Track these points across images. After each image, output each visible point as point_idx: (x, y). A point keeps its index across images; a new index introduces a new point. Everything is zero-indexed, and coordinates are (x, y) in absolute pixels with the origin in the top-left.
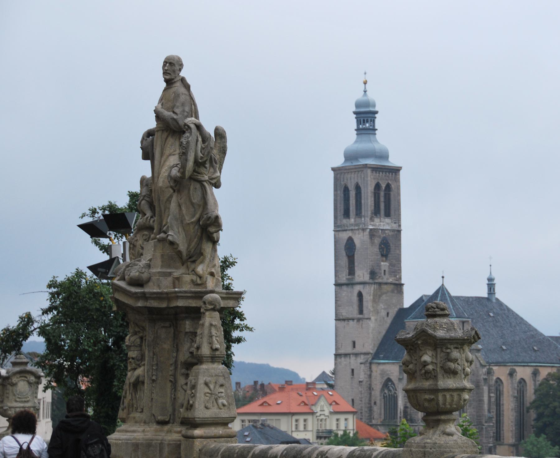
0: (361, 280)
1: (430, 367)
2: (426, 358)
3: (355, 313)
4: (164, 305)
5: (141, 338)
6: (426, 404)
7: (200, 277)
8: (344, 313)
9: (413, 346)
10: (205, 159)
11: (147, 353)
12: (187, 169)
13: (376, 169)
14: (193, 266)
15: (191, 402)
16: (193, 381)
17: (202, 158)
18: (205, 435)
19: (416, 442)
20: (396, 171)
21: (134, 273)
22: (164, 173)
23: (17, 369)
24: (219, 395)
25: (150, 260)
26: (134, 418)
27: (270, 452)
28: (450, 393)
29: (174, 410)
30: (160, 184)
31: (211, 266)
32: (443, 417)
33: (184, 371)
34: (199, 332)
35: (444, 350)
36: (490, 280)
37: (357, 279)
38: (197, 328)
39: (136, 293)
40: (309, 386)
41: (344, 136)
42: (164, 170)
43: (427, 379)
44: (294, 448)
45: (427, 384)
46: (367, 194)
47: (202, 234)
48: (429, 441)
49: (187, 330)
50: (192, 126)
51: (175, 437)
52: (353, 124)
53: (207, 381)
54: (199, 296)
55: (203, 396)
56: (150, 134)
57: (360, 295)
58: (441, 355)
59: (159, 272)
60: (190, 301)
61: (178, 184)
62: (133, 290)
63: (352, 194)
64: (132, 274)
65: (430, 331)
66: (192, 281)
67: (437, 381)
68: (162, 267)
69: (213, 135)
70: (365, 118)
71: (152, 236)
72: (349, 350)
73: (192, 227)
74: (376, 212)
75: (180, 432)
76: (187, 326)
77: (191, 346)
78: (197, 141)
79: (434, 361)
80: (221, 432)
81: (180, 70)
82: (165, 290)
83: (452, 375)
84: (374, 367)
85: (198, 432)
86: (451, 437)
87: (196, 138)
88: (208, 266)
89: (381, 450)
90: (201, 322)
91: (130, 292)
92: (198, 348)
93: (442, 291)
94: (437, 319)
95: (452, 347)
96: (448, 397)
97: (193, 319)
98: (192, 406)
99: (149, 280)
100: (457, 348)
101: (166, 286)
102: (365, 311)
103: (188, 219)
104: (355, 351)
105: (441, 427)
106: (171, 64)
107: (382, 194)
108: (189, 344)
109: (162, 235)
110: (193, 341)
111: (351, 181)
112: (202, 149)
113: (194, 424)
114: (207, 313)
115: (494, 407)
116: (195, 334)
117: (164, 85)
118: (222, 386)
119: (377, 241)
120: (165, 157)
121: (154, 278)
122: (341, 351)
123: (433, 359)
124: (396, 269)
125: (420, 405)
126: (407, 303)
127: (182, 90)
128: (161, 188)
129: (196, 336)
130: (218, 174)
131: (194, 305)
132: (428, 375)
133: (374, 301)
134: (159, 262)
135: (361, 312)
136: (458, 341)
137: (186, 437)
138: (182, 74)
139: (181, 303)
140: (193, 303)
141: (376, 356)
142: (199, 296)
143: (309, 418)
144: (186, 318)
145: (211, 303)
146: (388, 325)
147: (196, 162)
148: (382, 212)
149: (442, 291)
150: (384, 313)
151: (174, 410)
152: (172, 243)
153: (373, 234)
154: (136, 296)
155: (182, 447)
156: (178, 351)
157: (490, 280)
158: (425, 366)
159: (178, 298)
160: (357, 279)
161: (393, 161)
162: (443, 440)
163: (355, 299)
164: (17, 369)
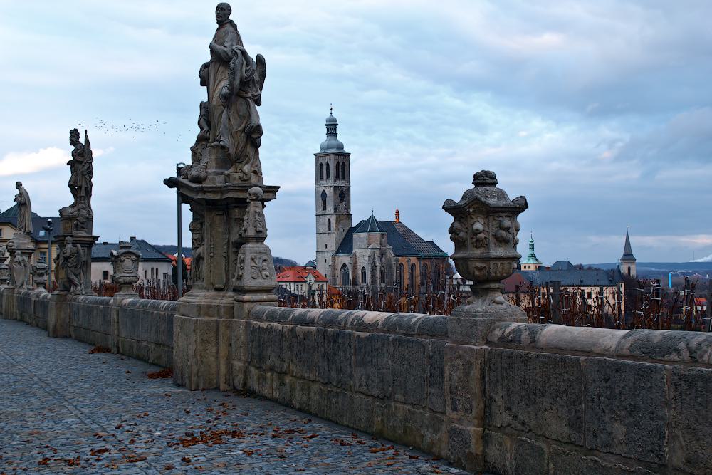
0: (330, 212)
1: (482, 235)
2: (478, 226)
3: (327, 230)
4: (218, 197)
5: (201, 224)
6: (477, 273)
7: (246, 175)
8: (322, 231)
9: (464, 214)
10: (249, 79)
11: (205, 235)
12: (235, 86)
13: (336, 154)
14: (240, 166)
15: (240, 273)
16: (242, 257)
17: (246, 78)
18: (252, 300)
19: (465, 310)
20: (348, 155)
21: (194, 173)
22: (217, 94)
23: (124, 251)
24: (263, 268)
25: (207, 163)
26: (198, 285)
27: (308, 315)
28: (501, 262)
29: (228, 280)
30: (214, 103)
31: (254, 165)
32: (492, 285)
33: (234, 249)
34: (246, 218)
35: (497, 219)
36: (397, 212)
37: (327, 212)
38: (244, 215)
39: (196, 188)
40: (304, 268)
41: (319, 138)
42: (216, 92)
43: (478, 248)
44: (330, 312)
45: (478, 252)
46: (334, 166)
47: (247, 140)
48: (479, 310)
49: (236, 217)
50: (238, 52)
51: (230, 300)
52: (325, 130)
53: (253, 257)
54: (245, 189)
55: (250, 269)
56: (206, 66)
57: (329, 220)
58: (494, 224)
59: (214, 172)
60: (239, 194)
61: (227, 100)
62: (194, 185)
63: (325, 167)
64: (193, 173)
65: (483, 199)
66: (240, 178)
67: (489, 250)
68: (216, 168)
69: (255, 60)
70: (332, 127)
71: (209, 144)
72: (324, 249)
73: (239, 134)
74: (337, 177)
75: (233, 297)
76: (236, 214)
77: (240, 230)
78: (243, 64)
79: (486, 229)
80: (220, 230)
81: (229, 14)
82: (219, 185)
83: (503, 244)
84: (248, 282)
85: (246, 297)
86: (500, 306)
87: (241, 61)
88: (251, 166)
89: (419, 317)
90: (247, 210)
91: (191, 187)
92: (245, 231)
93: (372, 218)
94: (487, 188)
95: (504, 215)
96: (499, 265)
97: (240, 208)
98: (241, 276)
99: (206, 178)
100: (508, 216)
101: (219, 181)
102: (332, 228)
103: (235, 128)
104: (327, 250)
105: (490, 296)
106: (222, 9)
107: (340, 168)
108: (238, 229)
109: (216, 143)
110: (241, 225)
111: (324, 161)
112: (247, 70)
113: (240, 290)
114: (252, 203)
115: (399, 278)
116: (243, 220)
117: (217, 26)
118: (265, 260)
119: (338, 192)
120: (217, 82)
121: (210, 177)
122: (320, 250)
123: (485, 227)
124: (348, 207)
125: (470, 274)
126: (353, 225)
127: (231, 29)
128: (214, 106)
129: (243, 221)
130: (259, 92)
131: (241, 197)
132: (479, 243)
133: (336, 223)
134: (213, 164)
135: (330, 229)
136: (510, 210)
137: (237, 301)
138: (231, 17)
139: (231, 195)
140: (241, 195)
141: (337, 252)
142: (245, 189)
143: (304, 284)
144: (236, 207)
145: (254, 194)
146: (343, 236)
147: (241, 81)
148: (341, 177)
149: (372, 218)
150: (341, 230)
151: (228, 280)
152: (223, 147)
153: (335, 188)
154: (197, 191)
155: (235, 309)
156: (229, 233)
157: (397, 212)
158: (476, 234)
159: (229, 191)
160: (327, 212)
161: (346, 150)
162: (493, 308)
163: (327, 223)
164: (124, 251)
